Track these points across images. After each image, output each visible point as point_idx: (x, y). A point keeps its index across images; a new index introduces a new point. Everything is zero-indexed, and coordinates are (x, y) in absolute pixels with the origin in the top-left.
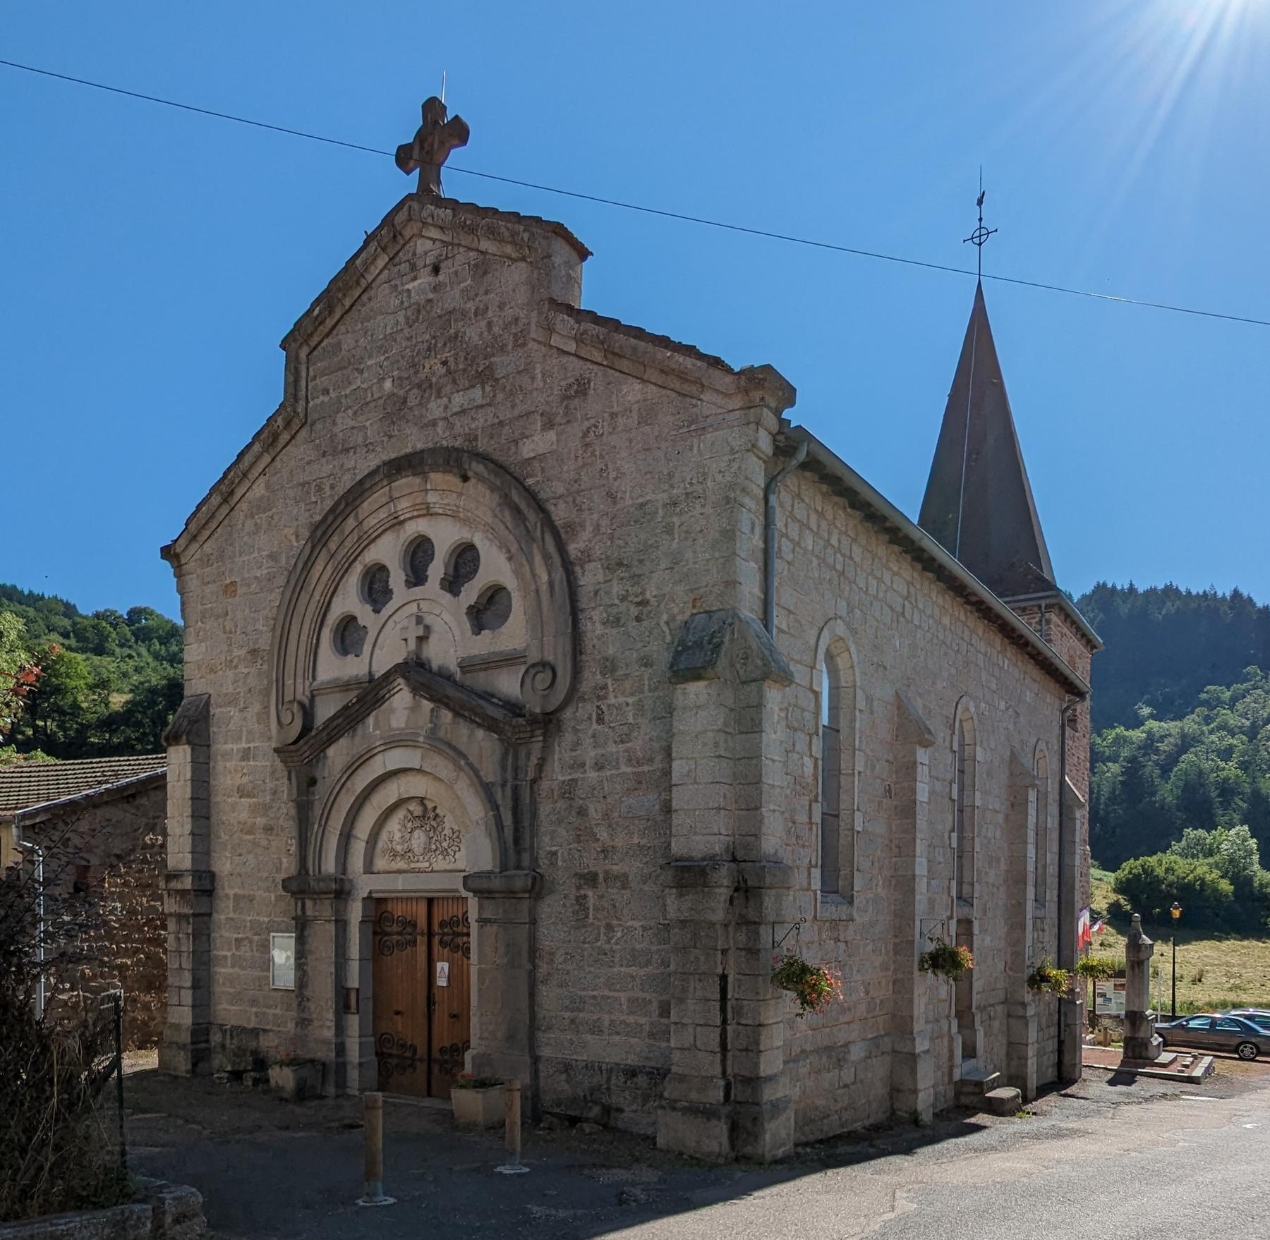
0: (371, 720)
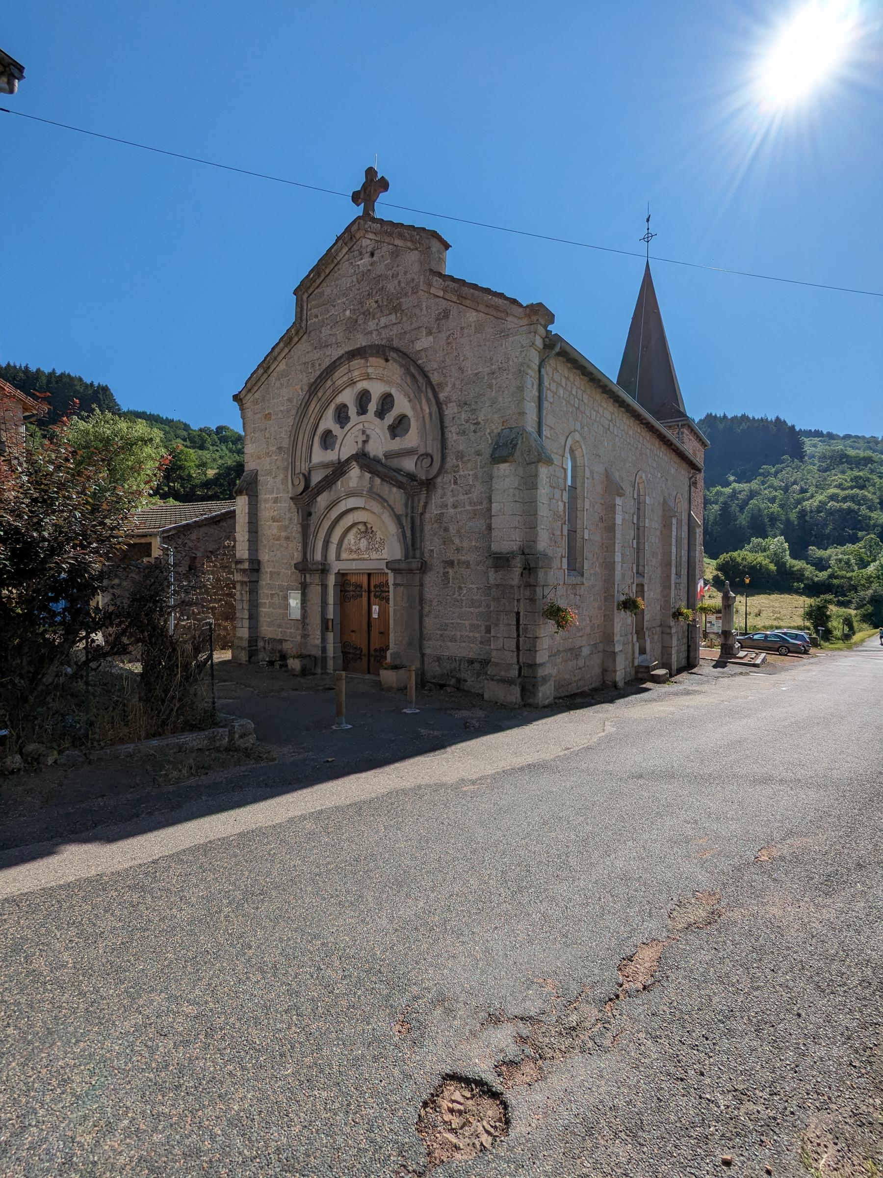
0: (339, 483)
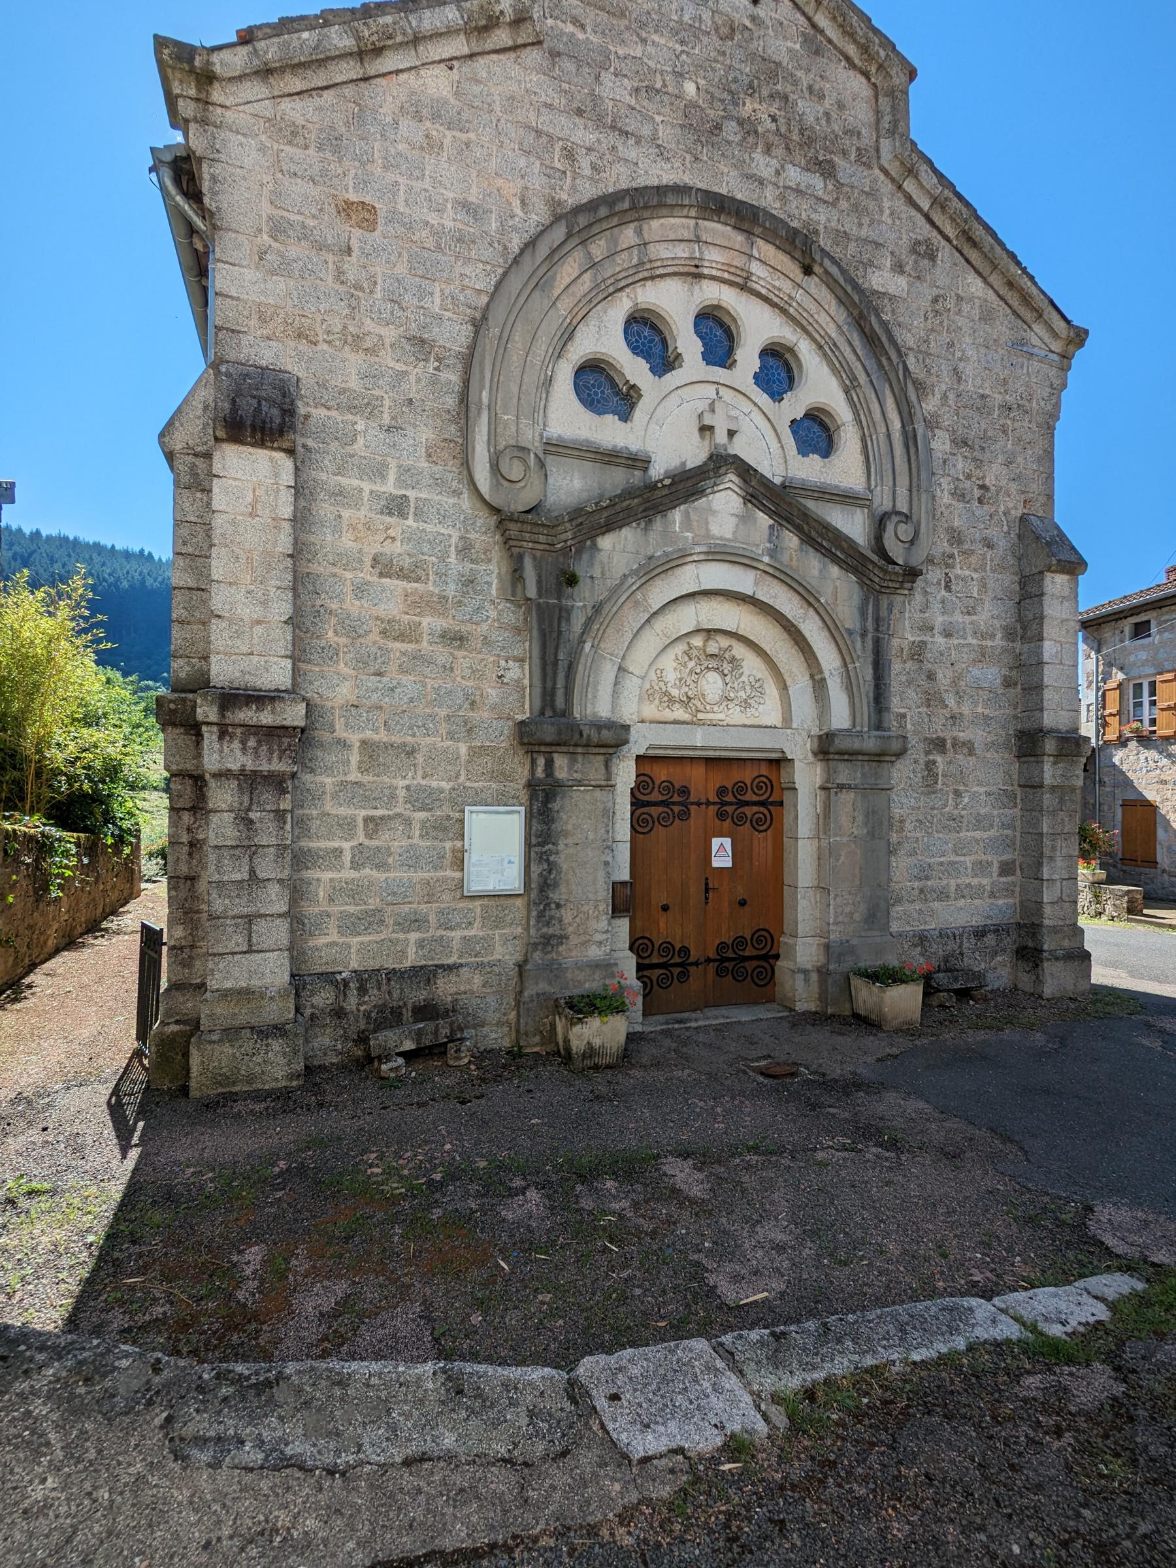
0: (677, 515)
